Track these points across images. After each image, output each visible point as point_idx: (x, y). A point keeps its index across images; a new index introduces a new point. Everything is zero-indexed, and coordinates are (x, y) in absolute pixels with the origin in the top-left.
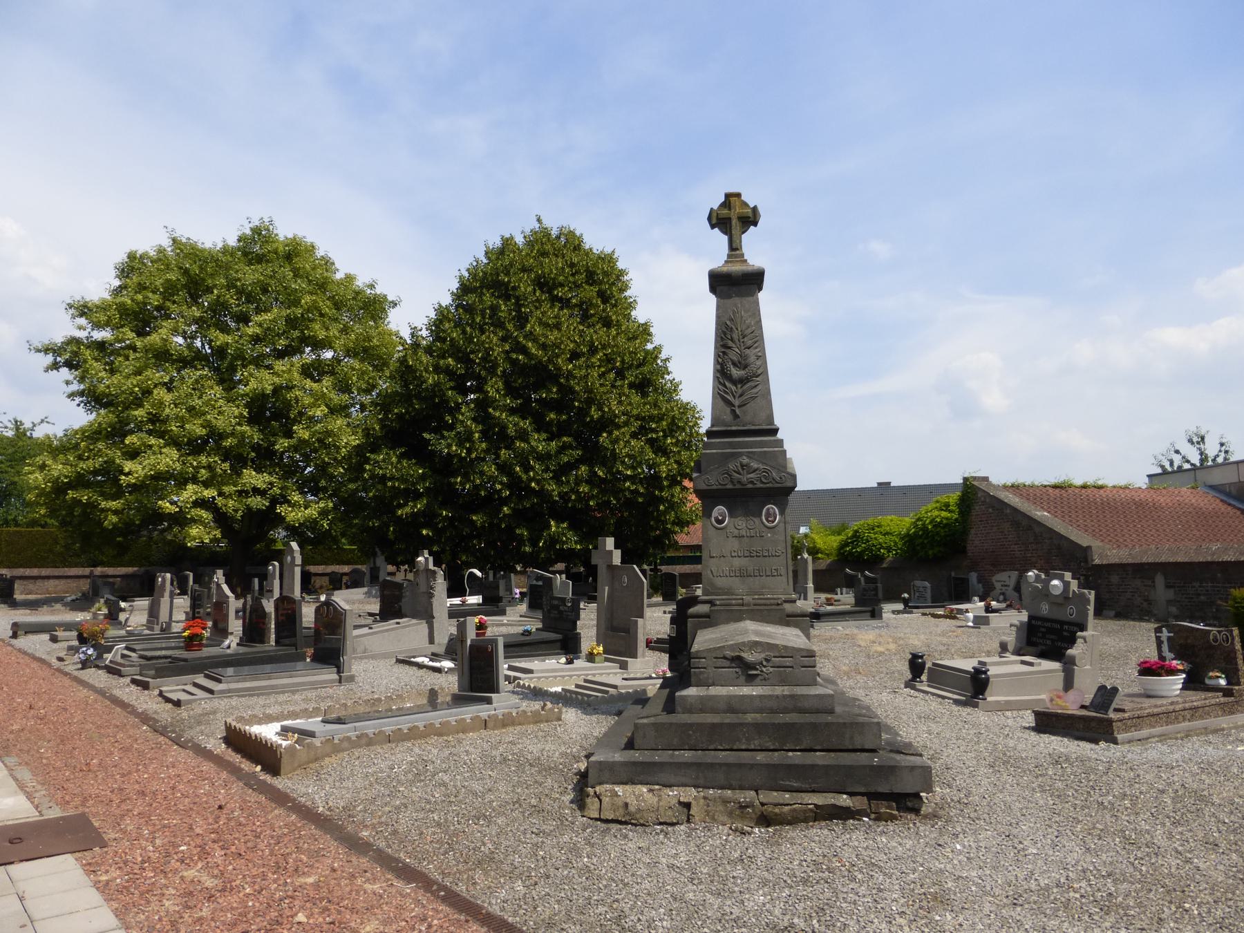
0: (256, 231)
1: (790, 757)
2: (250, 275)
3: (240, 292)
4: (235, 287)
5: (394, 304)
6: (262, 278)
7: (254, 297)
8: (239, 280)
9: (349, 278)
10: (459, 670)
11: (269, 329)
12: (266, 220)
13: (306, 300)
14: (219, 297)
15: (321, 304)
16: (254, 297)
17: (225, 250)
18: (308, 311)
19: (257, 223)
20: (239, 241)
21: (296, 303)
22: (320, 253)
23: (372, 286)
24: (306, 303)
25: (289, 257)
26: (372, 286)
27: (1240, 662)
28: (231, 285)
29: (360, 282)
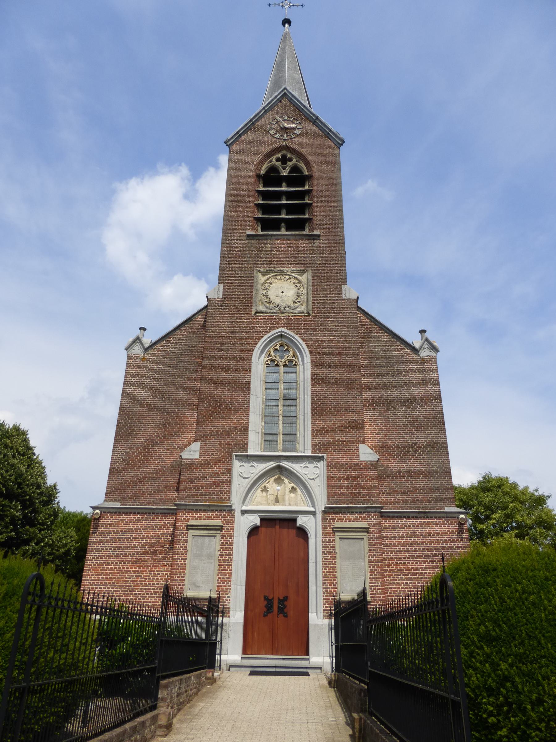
0: (484, 478)
1: (346, 678)
2: (486, 498)
3: (485, 506)
4: (482, 504)
5: (549, 497)
6: (491, 499)
7: (490, 509)
8: (483, 501)
9: (526, 488)
10: (367, 608)
11: (498, 520)
12: (487, 473)
13: (511, 505)
14: (477, 510)
15: (517, 506)
16: (490, 509)
17: (472, 487)
18: (513, 510)
19: (484, 475)
20: (478, 483)
21: (506, 508)
22: (521, 487)
23: (536, 490)
24: (511, 507)
25: (499, 487)
26: (536, 490)
27: (64, 741)
28: (480, 504)
29: (531, 489)
